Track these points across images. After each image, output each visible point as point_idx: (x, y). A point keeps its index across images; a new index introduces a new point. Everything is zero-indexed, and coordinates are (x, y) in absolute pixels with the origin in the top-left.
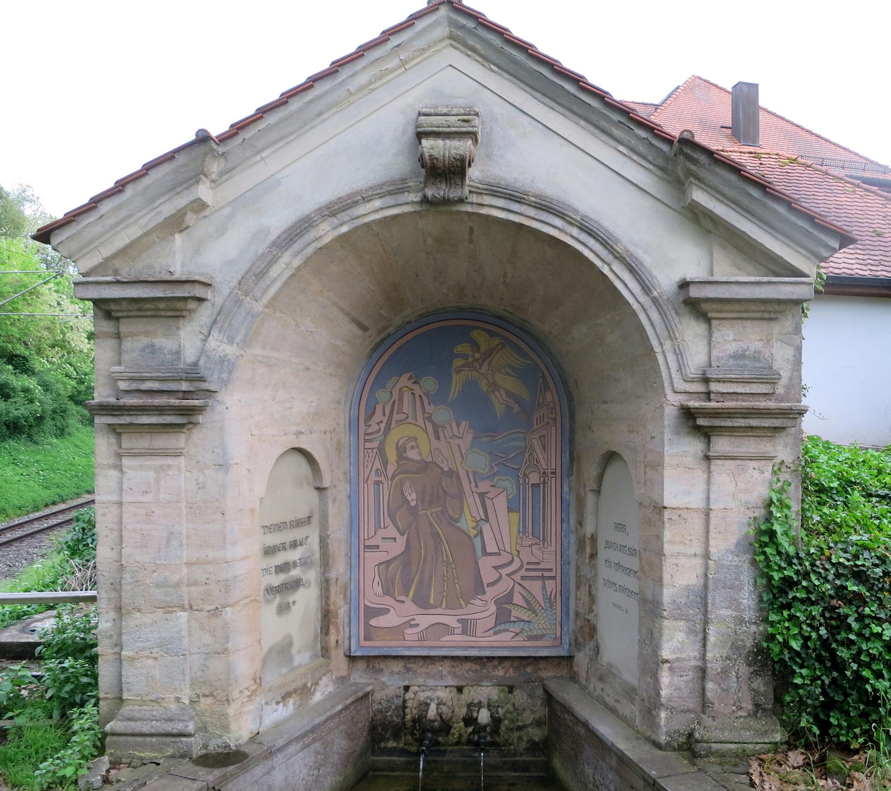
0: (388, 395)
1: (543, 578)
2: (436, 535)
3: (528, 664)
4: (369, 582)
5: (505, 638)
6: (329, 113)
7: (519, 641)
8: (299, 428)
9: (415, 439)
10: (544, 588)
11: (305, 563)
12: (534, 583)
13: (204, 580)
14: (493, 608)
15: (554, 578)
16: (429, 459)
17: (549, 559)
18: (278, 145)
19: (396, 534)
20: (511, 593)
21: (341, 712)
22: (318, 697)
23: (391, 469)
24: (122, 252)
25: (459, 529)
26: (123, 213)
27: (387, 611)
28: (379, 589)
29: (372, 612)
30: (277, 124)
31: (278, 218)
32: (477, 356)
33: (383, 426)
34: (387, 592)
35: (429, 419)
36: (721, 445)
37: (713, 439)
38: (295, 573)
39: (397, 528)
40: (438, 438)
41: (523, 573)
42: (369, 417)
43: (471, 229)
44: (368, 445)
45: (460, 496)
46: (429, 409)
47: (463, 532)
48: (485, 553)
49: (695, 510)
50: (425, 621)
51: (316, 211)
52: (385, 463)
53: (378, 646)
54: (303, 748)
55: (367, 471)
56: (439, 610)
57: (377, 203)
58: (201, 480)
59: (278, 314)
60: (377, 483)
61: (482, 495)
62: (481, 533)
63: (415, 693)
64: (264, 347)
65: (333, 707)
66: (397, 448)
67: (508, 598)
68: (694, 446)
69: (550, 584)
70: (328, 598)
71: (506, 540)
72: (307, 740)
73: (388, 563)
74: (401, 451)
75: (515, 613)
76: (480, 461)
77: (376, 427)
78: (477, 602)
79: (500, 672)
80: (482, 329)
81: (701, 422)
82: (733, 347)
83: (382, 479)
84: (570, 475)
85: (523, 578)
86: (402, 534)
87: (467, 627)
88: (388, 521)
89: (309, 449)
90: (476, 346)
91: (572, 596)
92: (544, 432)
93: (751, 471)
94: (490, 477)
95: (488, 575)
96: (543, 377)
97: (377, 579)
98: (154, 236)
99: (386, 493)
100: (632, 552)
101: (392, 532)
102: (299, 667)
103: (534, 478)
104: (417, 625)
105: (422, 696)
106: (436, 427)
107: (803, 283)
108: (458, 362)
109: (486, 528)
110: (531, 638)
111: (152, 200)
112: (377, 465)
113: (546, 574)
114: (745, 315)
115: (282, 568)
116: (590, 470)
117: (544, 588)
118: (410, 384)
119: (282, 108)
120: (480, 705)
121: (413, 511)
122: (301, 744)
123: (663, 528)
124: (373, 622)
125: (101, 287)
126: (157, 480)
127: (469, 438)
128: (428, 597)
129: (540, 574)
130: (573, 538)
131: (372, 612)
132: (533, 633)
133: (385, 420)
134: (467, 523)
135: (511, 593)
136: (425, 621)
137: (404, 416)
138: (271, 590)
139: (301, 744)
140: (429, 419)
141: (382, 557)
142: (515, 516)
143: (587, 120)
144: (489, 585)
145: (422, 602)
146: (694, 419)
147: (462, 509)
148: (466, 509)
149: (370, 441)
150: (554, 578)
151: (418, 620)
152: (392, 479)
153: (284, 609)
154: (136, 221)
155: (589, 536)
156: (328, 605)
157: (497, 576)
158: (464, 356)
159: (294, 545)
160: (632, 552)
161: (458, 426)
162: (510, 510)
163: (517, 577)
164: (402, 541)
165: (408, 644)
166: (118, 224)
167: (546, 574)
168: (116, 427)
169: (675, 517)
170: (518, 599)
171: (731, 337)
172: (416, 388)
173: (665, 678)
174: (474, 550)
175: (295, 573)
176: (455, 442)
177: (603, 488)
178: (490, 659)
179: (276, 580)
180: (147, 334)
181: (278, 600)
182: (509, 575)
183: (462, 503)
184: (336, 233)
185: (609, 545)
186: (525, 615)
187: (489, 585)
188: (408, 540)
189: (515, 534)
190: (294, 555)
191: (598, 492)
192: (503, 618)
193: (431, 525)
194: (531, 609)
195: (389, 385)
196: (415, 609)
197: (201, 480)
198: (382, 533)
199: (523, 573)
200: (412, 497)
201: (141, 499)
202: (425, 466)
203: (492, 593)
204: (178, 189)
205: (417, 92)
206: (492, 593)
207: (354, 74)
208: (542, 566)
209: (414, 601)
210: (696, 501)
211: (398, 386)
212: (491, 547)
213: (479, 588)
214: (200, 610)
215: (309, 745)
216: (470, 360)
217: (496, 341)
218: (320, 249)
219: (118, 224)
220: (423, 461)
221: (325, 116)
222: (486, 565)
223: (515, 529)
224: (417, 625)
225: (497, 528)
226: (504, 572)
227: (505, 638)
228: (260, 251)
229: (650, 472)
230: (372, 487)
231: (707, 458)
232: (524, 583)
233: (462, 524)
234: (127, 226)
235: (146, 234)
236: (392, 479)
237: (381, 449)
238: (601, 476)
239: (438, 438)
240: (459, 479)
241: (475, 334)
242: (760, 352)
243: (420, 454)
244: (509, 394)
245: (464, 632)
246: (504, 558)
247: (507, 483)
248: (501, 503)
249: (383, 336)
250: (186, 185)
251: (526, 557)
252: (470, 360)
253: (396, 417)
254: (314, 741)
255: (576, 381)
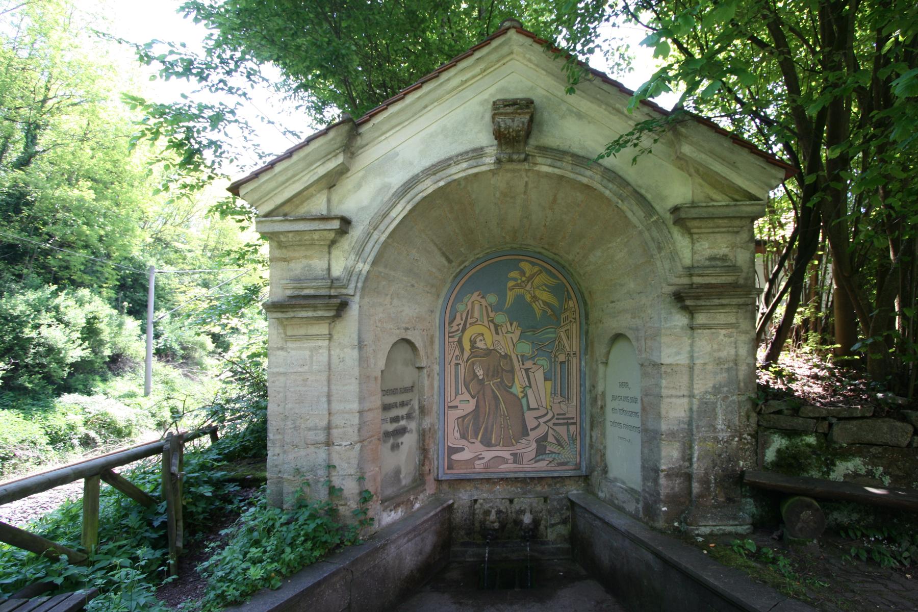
0: (464, 306)
1: (567, 424)
2: (496, 398)
3: (558, 482)
4: (451, 430)
5: (542, 464)
6: (432, 106)
7: (552, 467)
8: (407, 326)
9: (483, 335)
10: (568, 431)
11: (409, 416)
12: (561, 427)
13: (342, 425)
14: (534, 445)
15: (575, 424)
16: (492, 348)
17: (571, 410)
18: (397, 129)
19: (469, 398)
20: (546, 434)
21: (432, 517)
22: (417, 506)
23: (467, 354)
24: (289, 200)
25: (511, 393)
26: (290, 173)
27: (463, 449)
28: (457, 435)
29: (453, 451)
30: (398, 113)
31: (397, 178)
32: (524, 279)
33: (461, 327)
34: (463, 436)
35: (492, 321)
36: (701, 318)
37: (696, 315)
38: (403, 423)
39: (470, 394)
40: (497, 333)
41: (554, 421)
42: (451, 323)
43: (526, 182)
44: (451, 340)
45: (512, 371)
46: (492, 315)
47: (515, 395)
48: (529, 409)
49: (683, 365)
50: (488, 455)
51: (422, 172)
52: (462, 350)
53: (458, 472)
54: (408, 541)
55: (450, 357)
56: (498, 448)
57: (464, 165)
58: (342, 356)
59: (395, 244)
60: (457, 364)
61: (527, 370)
62: (526, 395)
63: (481, 504)
64: (386, 267)
65: (428, 513)
66: (471, 341)
67: (545, 438)
68: (680, 320)
69: (572, 428)
70: (424, 440)
71: (543, 400)
72: (410, 536)
73: (464, 417)
74: (473, 342)
75: (549, 448)
76: (526, 348)
77: (457, 328)
78: (524, 441)
79: (539, 488)
80: (527, 261)
81: (688, 303)
82: (708, 253)
83: (460, 362)
84: (586, 354)
85: (554, 424)
86: (473, 397)
87: (516, 458)
88: (464, 390)
89: (413, 340)
90: (523, 273)
91: (588, 435)
92: (568, 327)
93: (721, 337)
94: (532, 358)
95: (531, 423)
96: (568, 291)
97: (456, 428)
98: (312, 190)
99: (463, 371)
100: (634, 400)
101: (467, 396)
102: (405, 486)
103: (562, 358)
104: (483, 458)
105: (487, 506)
106: (496, 326)
107: (759, 205)
108: (511, 284)
109: (529, 392)
110: (560, 464)
111: (311, 164)
112: (457, 353)
113: (570, 421)
114: (717, 230)
115: (396, 419)
116: (600, 349)
117: (568, 431)
118: (479, 298)
119: (400, 102)
120: (523, 512)
121: (481, 382)
122: (406, 539)
123: (804, 272)
124: (454, 457)
125: (275, 224)
126: (311, 357)
127: (518, 333)
128: (491, 439)
129: (565, 421)
130: (588, 397)
131: (453, 451)
132: (567, 458)
133: (462, 323)
134: (517, 389)
135: (546, 434)
136: (488, 455)
137: (474, 320)
138: (387, 434)
139: (406, 539)
140: (492, 321)
141: (459, 413)
142: (549, 384)
143: (607, 104)
144: (532, 430)
145: (487, 443)
146: (684, 301)
147: (513, 379)
148: (516, 380)
149: (452, 337)
150: (575, 424)
151: (484, 454)
152: (467, 361)
153: (395, 447)
154: (300, 179)
155: (600, 393)
156: (424, 445)
157: (537, 423)
158: (515, 279)
159: (403, 404)
160: (634, 400)
161: (511, 325)
162: (546, 379)
163: (550, 424)
164: (473, 402)
165: (477, 471)
166: (287, 180)
167: (570, 421)
168: (286, 209)
169: (669, 370)
170: (551, 439)
171: (707, 246)
172: (483, 301)
173: (663, 481)
174: (522, 407)
175: (403, 423)
176: (510, 335)
177: (610, 361)
178: (532, 479)
179: (391, 427)
180: (306, 257)
181: (391, 441)
182: (545, 423)
183: (513, 375)
184: (435, 187)
185: (614, 398)
186: (556, 449)
187: (532, 430)
188: (477, 401)
189: (548, 396)
190: (402, 412)
191: (606, 363)
192: (541, 450)
193: (493, 390)
194: (560, 444)
195: (465, 300)
196: (481, 446)
197: (342, 356)
198: (460, 397)
199: (554, 421)
200: (480, 373)
201: (300, 369)
202: (488, 352)
203: (533, 435)
204: (329, 157)
205: (492, 90)
206: (533, 435)
207: (448, 80)
208: (567, 416)
209: (481, 442)
210: (683, 359)
211: (472, 300)
212: (533, 405)
213: (525, 432)
214: (340, 445)
215: (412, 539)
216: (519, 281)
217: (536, 269)
218: (425, 197)
219: (287, 180)
220: (488, 349)
221: (429, 108)
222: (529, 417)
223: (549, 391)
224: (483, 458)
225: (536, 390)
226: (542, 420)
227: (542, 464)
228: (385, 199)
229: (649, 343)
230: (453, 367)
231: (692, 328)
232: (554, 427)
233: (513, 390)
234: (294, 182)
235: (306, 188)
236: (467, 361)
237: (460, 342)
238: (609, 353)
239: (497, 333)
240: (511, 360)
241: (523, 265)
242: (726, 256)
243: (486, 344)
244: (545, 303)
245: (515, 462)
246: (542, 412)
247: (543, 362)
248: (539, 375)
249: (462, 267)
250: (334, 154)
251: (557, 410)
252: (519, 281)
253: (469, 321)
254: (415, 536)
255: (590, 292)
